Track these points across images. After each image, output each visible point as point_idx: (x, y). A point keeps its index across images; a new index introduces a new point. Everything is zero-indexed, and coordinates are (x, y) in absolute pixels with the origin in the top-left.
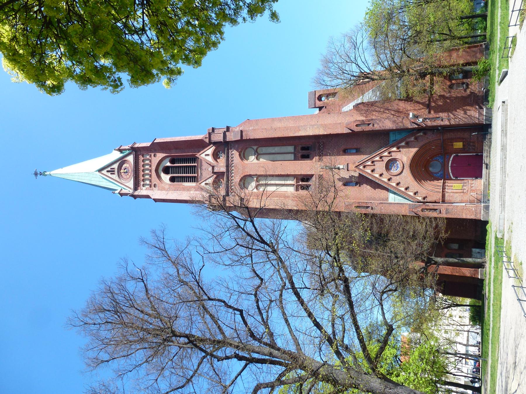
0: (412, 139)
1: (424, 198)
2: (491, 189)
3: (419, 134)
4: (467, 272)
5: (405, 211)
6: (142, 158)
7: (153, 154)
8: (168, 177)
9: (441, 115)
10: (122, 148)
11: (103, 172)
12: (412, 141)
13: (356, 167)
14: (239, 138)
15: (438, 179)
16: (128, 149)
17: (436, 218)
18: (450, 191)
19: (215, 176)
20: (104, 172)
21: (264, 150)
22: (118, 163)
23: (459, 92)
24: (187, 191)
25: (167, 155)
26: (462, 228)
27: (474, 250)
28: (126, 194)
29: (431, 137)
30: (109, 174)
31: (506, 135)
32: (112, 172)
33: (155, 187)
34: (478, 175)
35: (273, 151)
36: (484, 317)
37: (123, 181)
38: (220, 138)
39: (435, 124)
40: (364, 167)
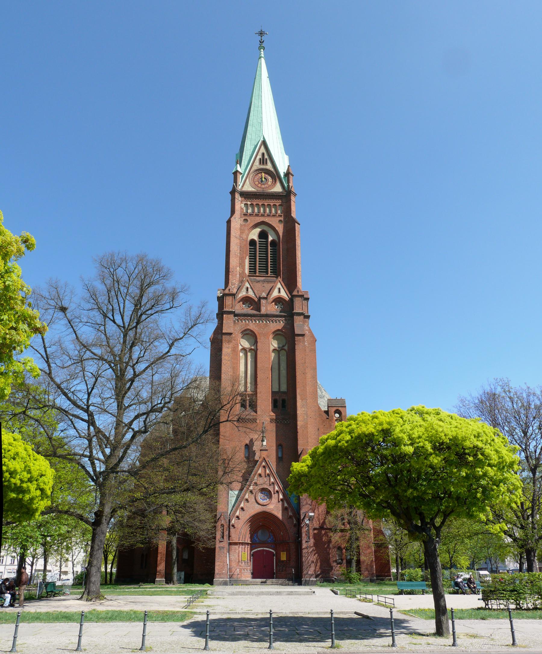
0: (290, 514)
1: (233, 526)
2: (243, 586)
3: (294, 520)
4: (161, 567)
5: (221, 508)
6: (277, 204)
7: (282, 219)
8: (256, 238)
9: (312, 541)
10: (291, 176)
11: (263, 147)
12: (288, 513)
13: (264, 459)
14: (297, 332)
15: (251, 538)
16: (288, 186)
17: (215, 538)
18: (240, 549)
19: (256, 300)
20: (263, 150)
21: (284, 358)
22: (272, 170)
23: (334, 555)
24: (241, 264)
25: (281, 237)
26: (204, 562)
27: (183, 573)
28: (235, 181)
29: (292, 531)
30: (260, 156)
31: (289, 594)
32: (263, 161)
33: (245, 220)
34: (255, 575)
35: (282, 369)
36: (121, 585)
37: (251, 176)
38: (297, 310)
39: (304, 535)
40: (264, 467)
